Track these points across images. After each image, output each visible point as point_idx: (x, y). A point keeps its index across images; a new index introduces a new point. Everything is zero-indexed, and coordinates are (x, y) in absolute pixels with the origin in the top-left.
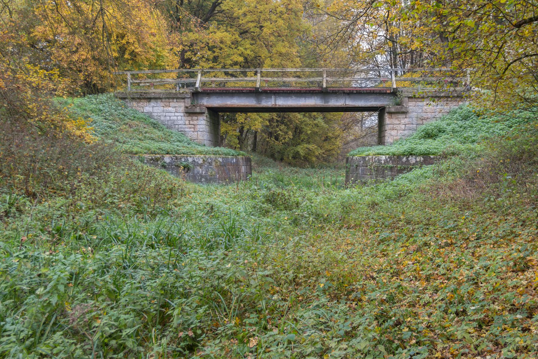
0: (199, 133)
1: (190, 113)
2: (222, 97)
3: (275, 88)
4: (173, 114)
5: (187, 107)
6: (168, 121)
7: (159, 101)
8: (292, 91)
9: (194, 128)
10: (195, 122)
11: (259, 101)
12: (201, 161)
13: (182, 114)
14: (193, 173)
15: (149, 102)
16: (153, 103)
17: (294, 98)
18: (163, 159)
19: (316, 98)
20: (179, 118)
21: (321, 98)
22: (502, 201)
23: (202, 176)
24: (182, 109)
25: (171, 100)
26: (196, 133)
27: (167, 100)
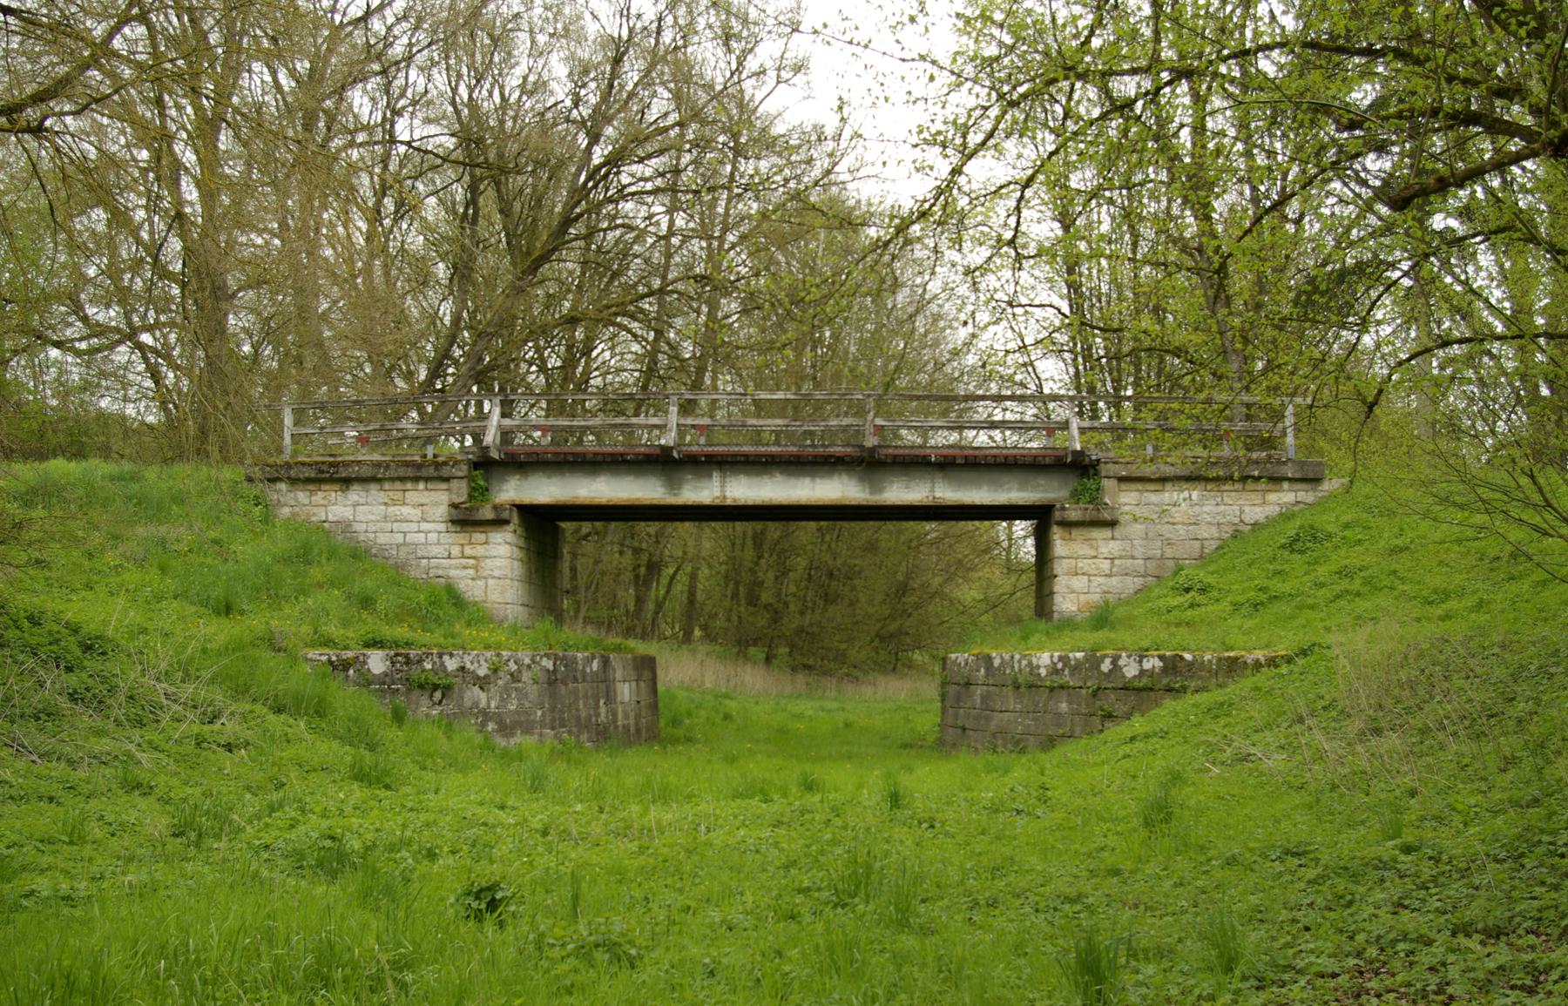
0: (491, 582)
1: (464, 520)
2: (562, 474)
4: (414, 527)
5: (454, 506)
6: (398, 546)
7: (374, 487)
8: (746, 456)
9: (476, 568)
10: (480, 551)
13: (442, 527)
14: (460, 706)
16: (355, 494)
17: (779, 478)
18: (365, 663)
19: (845, 478)
20: (433, 537)
21: (862, 480)
24: (442, 511)
25: (409, 485)
26: (481, 583)
27: (398, 485)
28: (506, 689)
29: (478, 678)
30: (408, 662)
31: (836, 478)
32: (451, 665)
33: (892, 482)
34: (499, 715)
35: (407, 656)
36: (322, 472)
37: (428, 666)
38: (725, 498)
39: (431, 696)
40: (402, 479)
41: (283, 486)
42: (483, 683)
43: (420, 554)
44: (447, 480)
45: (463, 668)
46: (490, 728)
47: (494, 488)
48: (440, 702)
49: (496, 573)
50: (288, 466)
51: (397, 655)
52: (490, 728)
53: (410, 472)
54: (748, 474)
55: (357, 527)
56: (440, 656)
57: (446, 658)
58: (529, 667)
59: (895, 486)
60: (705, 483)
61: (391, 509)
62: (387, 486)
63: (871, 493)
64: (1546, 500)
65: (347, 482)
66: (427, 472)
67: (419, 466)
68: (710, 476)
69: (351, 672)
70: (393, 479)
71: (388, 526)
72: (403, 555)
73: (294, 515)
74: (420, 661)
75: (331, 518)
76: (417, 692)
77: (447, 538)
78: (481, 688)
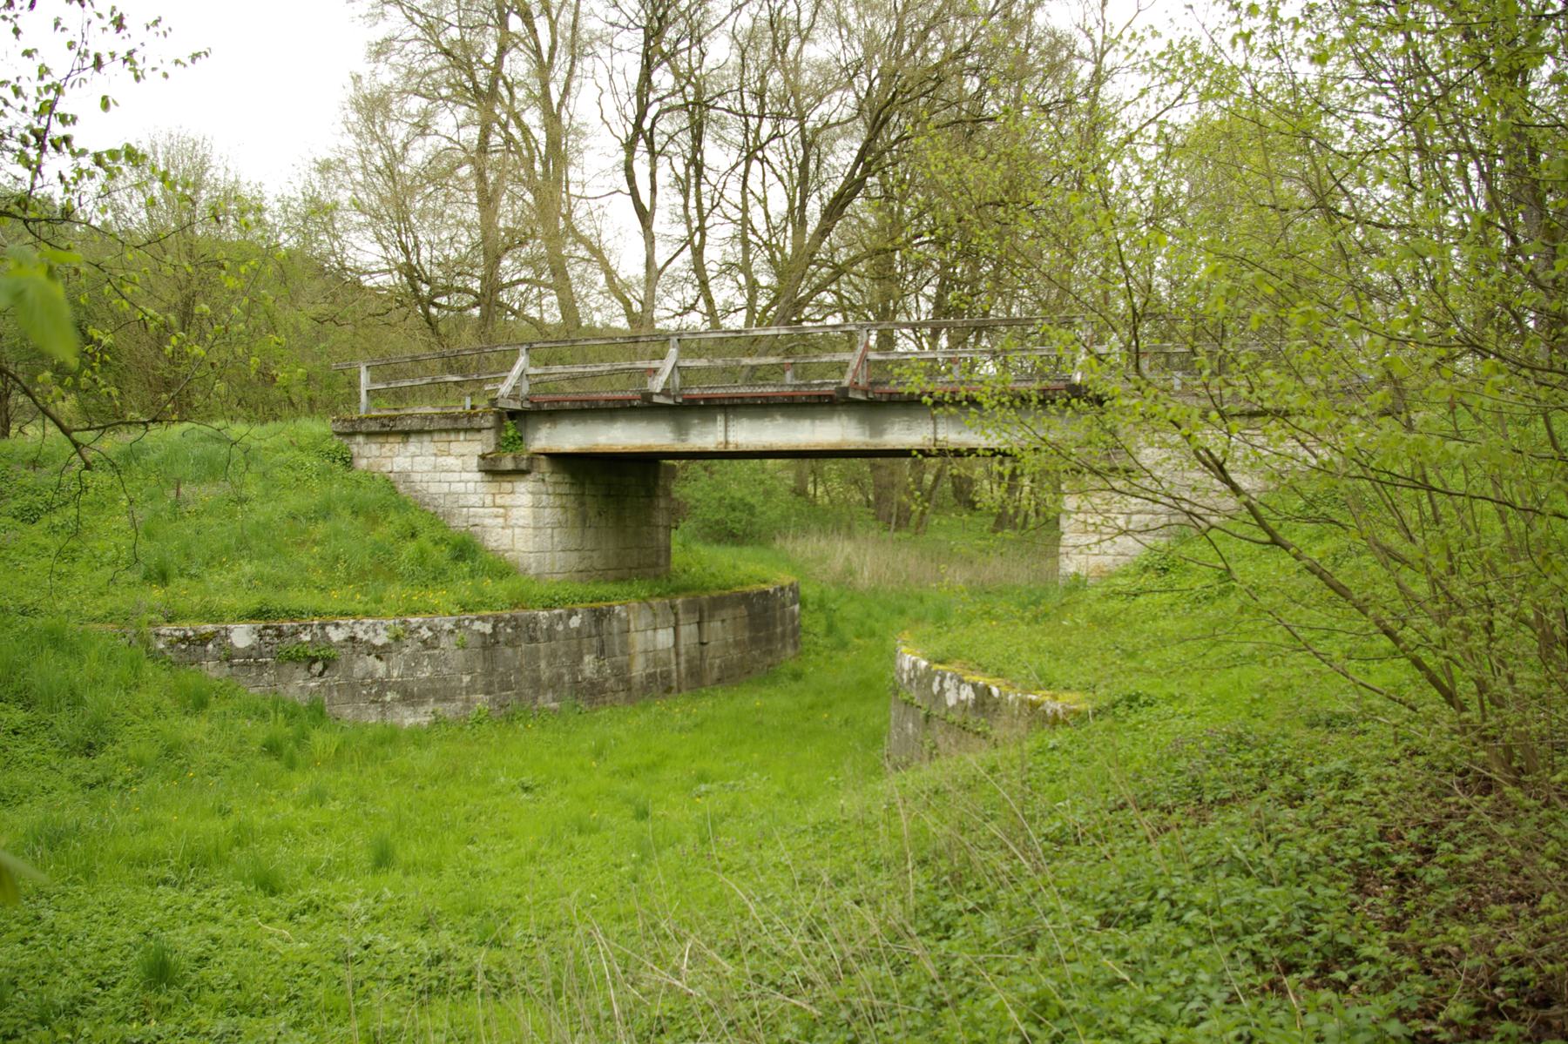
0: (517, 530)
1: (492, 470)
2: (585, 421)
3: (720, 391)
4: (456, 476)
5: (483, 457)
6: (446, 495)
7: (426, 438)
8: (766, 397)
9: (505, 517)
10: (507, 500)
11: (681, 431)
12: (381, 639)
13: (478, 476)
14: (347, 677)
15: (405, 442)
16: (413, 446)
17: (780, 421)
18: (227, 637)
19: (844, 419)
20: (471, 486)
21: (861, 421)
22: (1474, 82)
23: (384, 686)
24: (474, 462)
25: (453, 437)
26: (509, 532)
27: (444, 436)
28: (415, 658)
29: (374, 647)
30: (280, 634)
31: (836, 419)
32: (336, 635)
33: (893, 424)
34: (402, 683)
35: (279, 629)
36: (383, 425)
37: (306, 637)
38: (727, 443)
39: (309, 669)
40: (447, 431)
41: (360, 439)
42: (381, 653)
43: (461, 503)
44: (479, 430)
45: (353, 639)
46: (388, 698)
47: (529, 436)
48: (321, 674)
49: (521, 522)
50: (361, 420)
51: (266, 628)
52: (388, 698)
53: (449, 424)
54: (751, 417)
55: (416, 477)
56: (323, 627)
57: (330, 630)
58: (451, 632)
59: (897, 427)
60: (710, 427)
61: (440, 459)
62: (436, 437)
63: (871, 436)
64: (1270, 532)
65: (406, 434)
66: (458, 425)
67: (455, 418)
68: (715, 420)
69: (210, 646)
70: (441, 431)
71: (437, 476)
72: (448, 504)
73: (370, 465)
74: (295, 633)
75: (396, 469)
76: (289, 665)
77: (482, 488)
78: (378, 657)
